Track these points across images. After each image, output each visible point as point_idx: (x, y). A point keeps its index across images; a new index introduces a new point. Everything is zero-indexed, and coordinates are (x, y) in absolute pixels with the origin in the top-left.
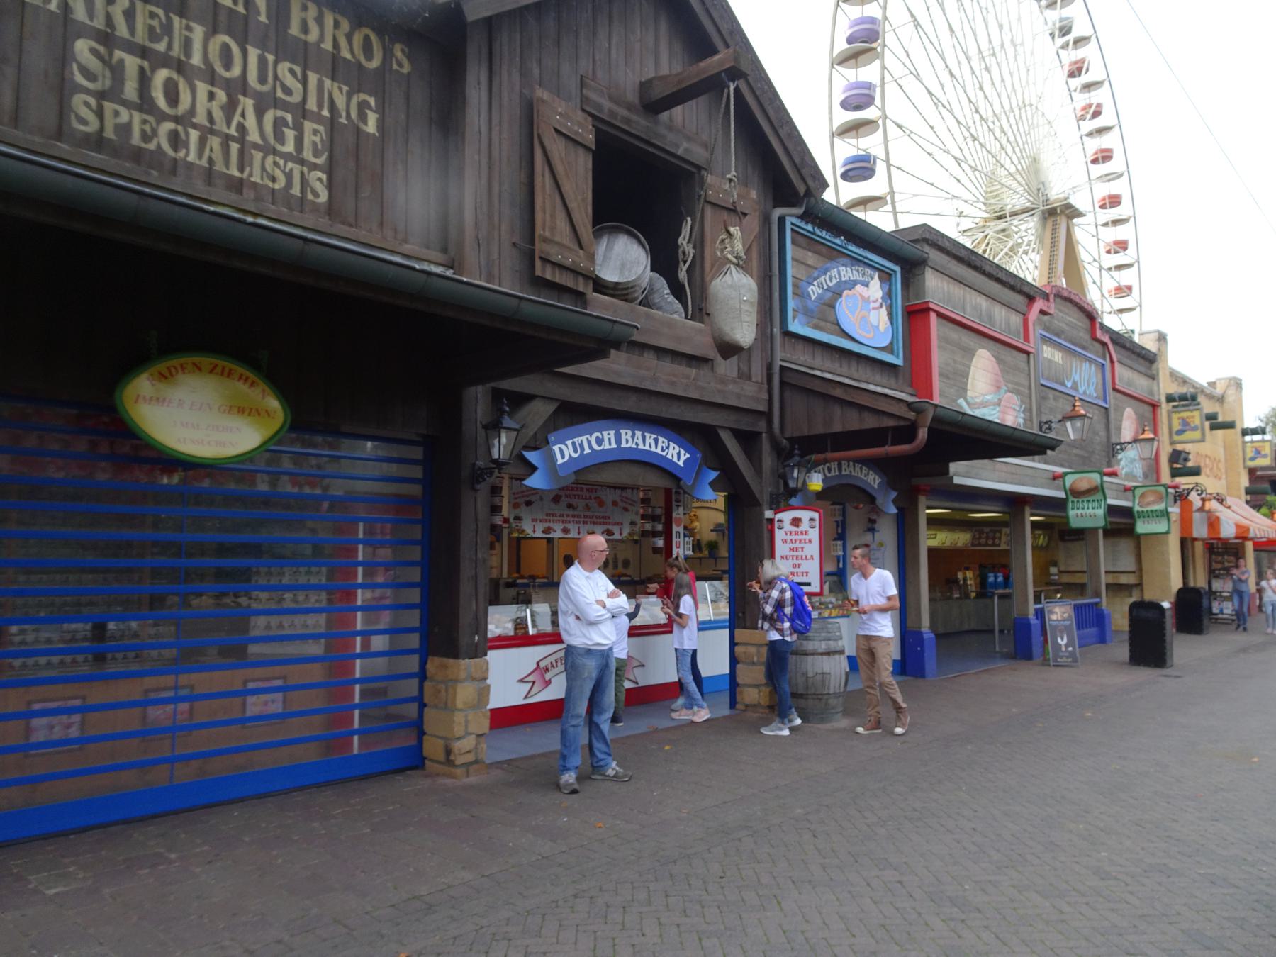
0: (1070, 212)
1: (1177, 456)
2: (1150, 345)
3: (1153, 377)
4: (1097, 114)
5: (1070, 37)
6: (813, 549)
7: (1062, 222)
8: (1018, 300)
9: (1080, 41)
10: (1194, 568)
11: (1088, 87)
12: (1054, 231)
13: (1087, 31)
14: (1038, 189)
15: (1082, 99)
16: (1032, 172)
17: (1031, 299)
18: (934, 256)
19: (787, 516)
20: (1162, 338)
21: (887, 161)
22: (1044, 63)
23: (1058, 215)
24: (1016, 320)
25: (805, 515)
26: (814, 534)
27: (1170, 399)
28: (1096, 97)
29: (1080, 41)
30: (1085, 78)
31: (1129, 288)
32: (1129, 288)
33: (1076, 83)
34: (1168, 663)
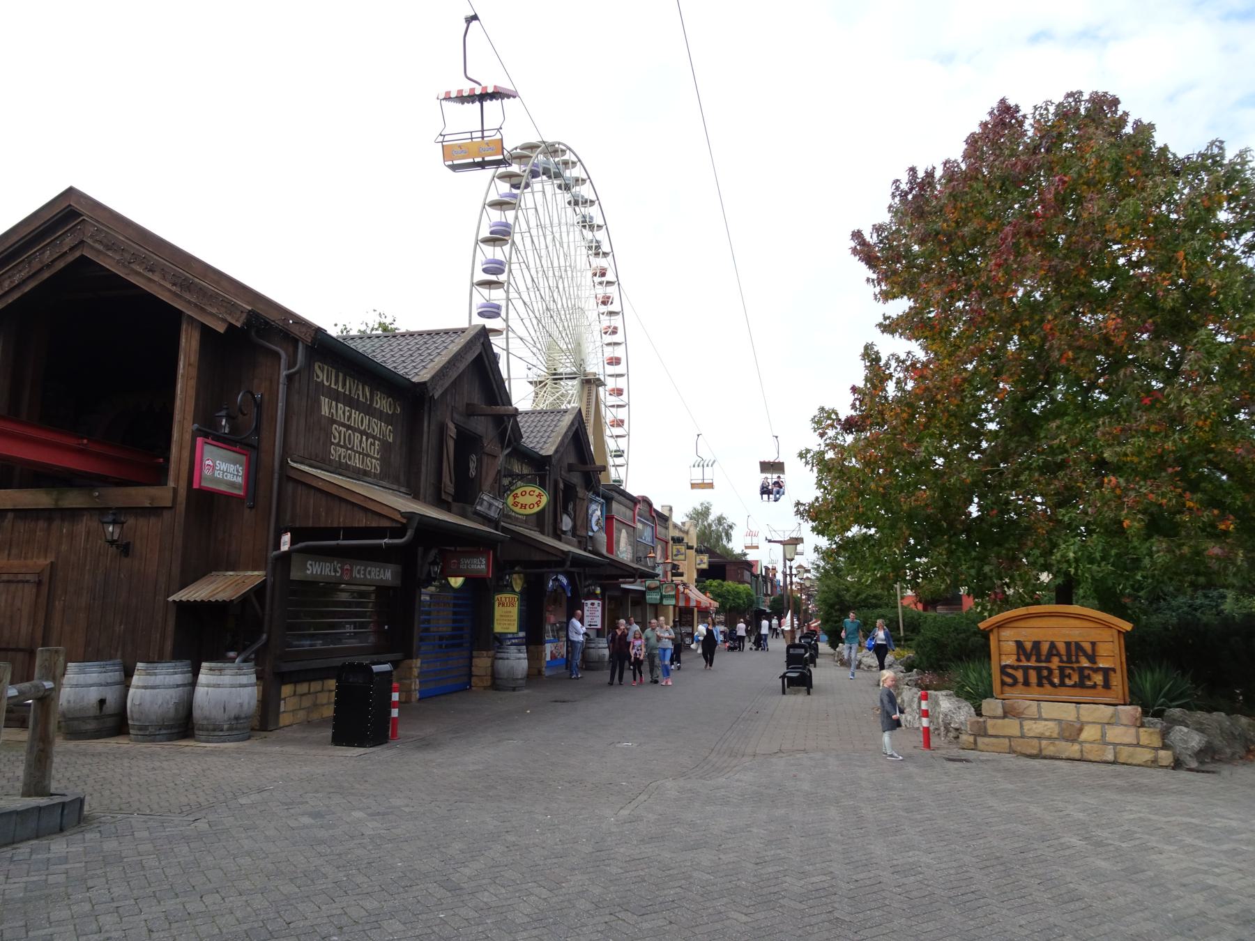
0: (599, 383)
1: (675, 567)
2: (667, 514)
3: (667, 528)
4: (614, 332)
5: (604, 279)
6: (599, 613)
7: (594, 388)
8: (631, 504)
9: (609, 283)
10: (81, 452)
11: (611, 313)
12: (589, 394)
13: (613, 279)
14: (580, 364)
15: (606, 321)
16: (577, 351)
17: (635, 504)
18: (615, 495)
19: (589, 602)
20: (671, 509)
21: (507, 350)
22: (588, 293)
23: (591, 383)
24: (629, 513)
25: (596, 602)
26: (600, 609)
27: (673, 539)
28: (616, 321)
29: (609, 283)
30: (611, 308)
31: (622, 421)
32: (622, 421)
33: (603, 309)
34: (394, 735)
